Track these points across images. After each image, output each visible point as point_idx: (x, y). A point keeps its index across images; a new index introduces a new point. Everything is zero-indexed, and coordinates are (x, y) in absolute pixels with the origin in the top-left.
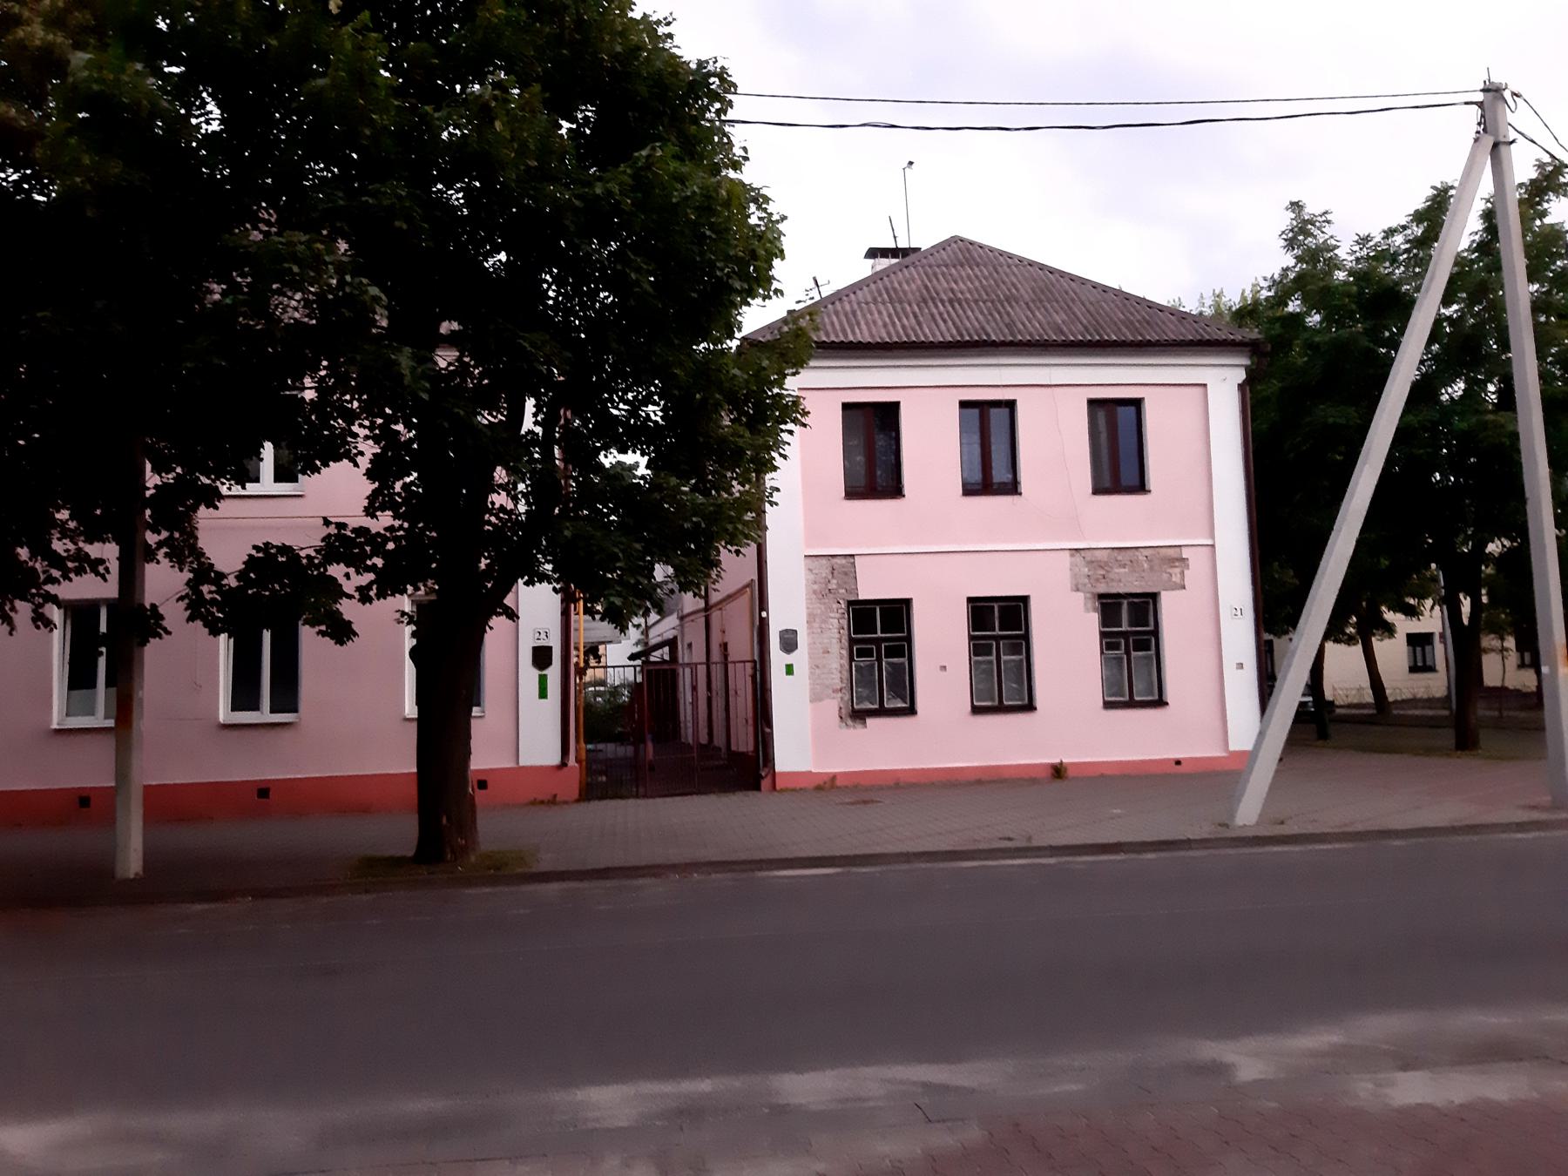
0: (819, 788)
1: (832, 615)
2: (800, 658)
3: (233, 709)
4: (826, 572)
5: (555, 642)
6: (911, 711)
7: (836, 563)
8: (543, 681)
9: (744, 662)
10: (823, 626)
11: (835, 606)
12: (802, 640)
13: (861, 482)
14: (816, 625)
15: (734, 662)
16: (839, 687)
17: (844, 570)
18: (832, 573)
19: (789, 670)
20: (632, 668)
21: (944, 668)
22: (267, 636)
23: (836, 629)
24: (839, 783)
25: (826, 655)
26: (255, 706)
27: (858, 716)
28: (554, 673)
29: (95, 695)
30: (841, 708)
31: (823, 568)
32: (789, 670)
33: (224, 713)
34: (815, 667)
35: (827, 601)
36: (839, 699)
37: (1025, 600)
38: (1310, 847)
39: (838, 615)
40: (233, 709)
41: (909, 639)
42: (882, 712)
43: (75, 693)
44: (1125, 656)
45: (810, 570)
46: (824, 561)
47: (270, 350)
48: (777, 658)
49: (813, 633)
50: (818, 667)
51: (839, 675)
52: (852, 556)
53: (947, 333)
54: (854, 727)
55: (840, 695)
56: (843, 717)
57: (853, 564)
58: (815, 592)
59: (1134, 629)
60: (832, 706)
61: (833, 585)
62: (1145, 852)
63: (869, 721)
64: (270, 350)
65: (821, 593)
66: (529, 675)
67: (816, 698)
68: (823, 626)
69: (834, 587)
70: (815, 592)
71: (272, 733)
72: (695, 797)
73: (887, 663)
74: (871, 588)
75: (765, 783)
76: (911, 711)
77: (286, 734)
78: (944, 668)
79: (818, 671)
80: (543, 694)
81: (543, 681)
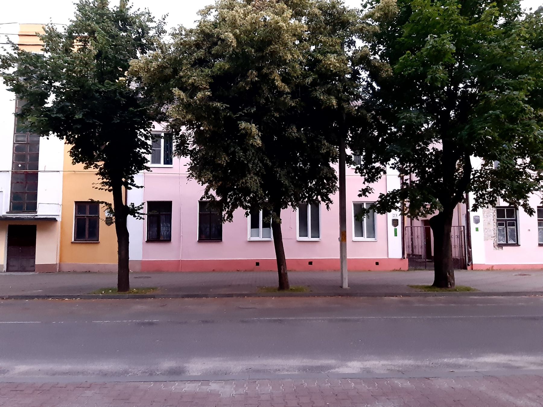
0: (488, 270)
2: (480, 225)
8: (396, 230)
19: (477, 229)
24: (494, 268)
27: (500, 246)
28: (399, 228)
32: (477, 229)
37: (172, 202)
60: (491, 242)
66: (391, 228)
67: (486, 239)
77: (317, 245)
81: (396, 230)
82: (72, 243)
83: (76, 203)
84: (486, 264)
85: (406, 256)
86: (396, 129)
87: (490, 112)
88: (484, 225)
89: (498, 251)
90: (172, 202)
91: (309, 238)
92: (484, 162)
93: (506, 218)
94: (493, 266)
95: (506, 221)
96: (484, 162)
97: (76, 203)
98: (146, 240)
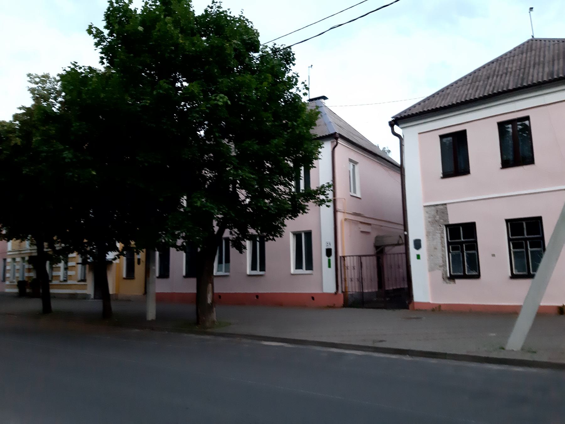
0: (433, 310)
1: (437, 232)
2: (423, 251)
3: (296, 269)
4: (433, 213)
5: (332, 247)
6: (478, 276)
7: (439, 208)
8: (329, 261)
9: (401, 254)
10: (434, 237)
11: (438, 227)
12: (424, 244)
13: (451, 168)
14: (430, 237)
15: (390, 254)
16: (442, 265)
17: (442, 211)
18: (437, 213)
19: (418, 257)
20: (397, 255)
21: (493, 255)
22: (157, 253)
23: (443, 236)
24: (442, 308)
25: (435, 250)
26: (221, 271)
27: (452, 278)
28: (332, 258)
29: (222, 266)
30: (443, 274)
31: (433, 211)
32: (418, 257)
33: (249, 271)
34: (430, 255)
35: (435, 225)
36: (442, 270)
37: (540, 218)
38: (202, 337)
39: (440, 232)
40: (296, 269)
41: (476, 242)
42: (465, 277)
43: (219, 265)
44: (461, 254)
45: (427, 212)
46: (433, 208)
47: (295, 149)
48: (413, 252)
49: (430, 240)
50: (432, 256)
51: (441, 259)
52: (445, 204)
53: (488, 90)
54: (450, 283)
55: (442, 268)
56: (444, 278)
57: (446, 208)
58: (429, 222)
59: (466, 240)
60: (439, 273)
61: (438, 218)
62: (261, 340)
63: (457, 281)
64: (295, 149)
65: (432, 222)
66: (325, 259)
67: (431, 269)
68: (434, 237)
69: (438, 219)
70: (429, 222)
71: (258, 278)
72: (384, 310)
73: (467, 253)
74: (453, 220)
75: (410, 306)
76: (478, 276)
77: (262, 278)
78: (493, 255)
79: (432, 258)
80: (329, 266)
81: (329, 261)
82: (124, 279)
83: (507, 221)
84: (431, 302)
85: (340, 292)
86: (297, 132)
87: (191, 54)
88: (429, 250)
89: (449, 285)
90: (540, 218)
91: (258, 272)
92: (314, 160)
93: (526, 236)
94: (440, 306)
95: (526, 239)
96: (314, 160)
97: (507, 221)
98: (184, 274)
